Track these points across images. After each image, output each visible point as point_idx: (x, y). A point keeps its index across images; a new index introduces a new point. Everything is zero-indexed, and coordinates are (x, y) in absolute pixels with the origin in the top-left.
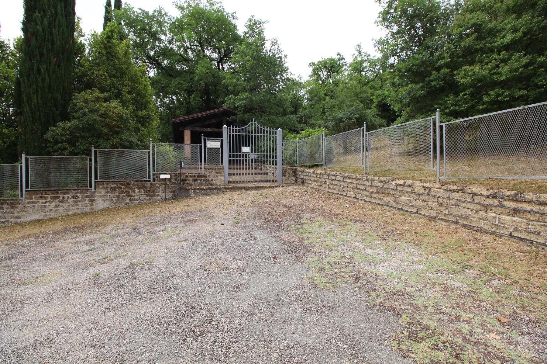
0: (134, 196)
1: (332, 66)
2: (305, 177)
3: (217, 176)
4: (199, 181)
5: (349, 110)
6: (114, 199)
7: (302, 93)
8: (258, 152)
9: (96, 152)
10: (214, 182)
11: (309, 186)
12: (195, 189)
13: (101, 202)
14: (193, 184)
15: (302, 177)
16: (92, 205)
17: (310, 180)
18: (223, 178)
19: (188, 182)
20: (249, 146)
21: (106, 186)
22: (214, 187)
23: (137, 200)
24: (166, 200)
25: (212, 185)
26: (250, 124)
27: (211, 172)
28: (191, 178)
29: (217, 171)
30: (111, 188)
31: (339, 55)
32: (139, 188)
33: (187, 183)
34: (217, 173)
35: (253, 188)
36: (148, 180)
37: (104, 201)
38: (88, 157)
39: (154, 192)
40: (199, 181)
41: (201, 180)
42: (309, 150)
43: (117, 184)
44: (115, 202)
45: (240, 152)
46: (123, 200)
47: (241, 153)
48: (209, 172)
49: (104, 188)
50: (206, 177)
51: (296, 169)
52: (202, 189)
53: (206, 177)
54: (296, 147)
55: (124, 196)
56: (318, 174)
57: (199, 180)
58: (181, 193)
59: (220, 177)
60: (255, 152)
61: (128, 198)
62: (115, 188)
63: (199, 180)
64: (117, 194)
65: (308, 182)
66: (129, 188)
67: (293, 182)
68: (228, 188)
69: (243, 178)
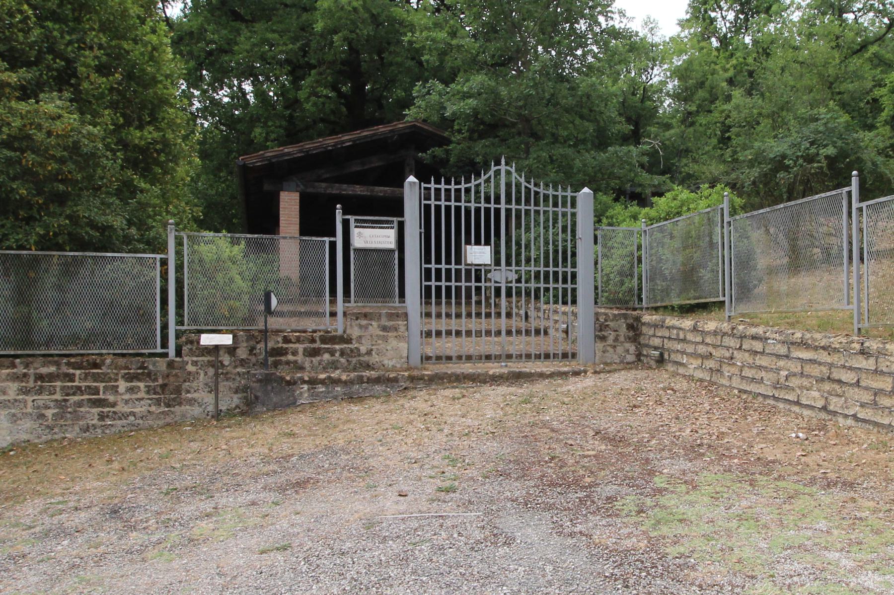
0: (114, 405)
2: (668, 344)
4: (326, 356)
6: (49, 413)
7: (657, 75)
8: (518, 263)
10: (374, 359)
11: (681, 370)
12: (313, 382)
14: (307, 365)
15: (657, 342)
19: (290, 357)
20: (487, 243)
21: (21, 370)
22: (374, 374)
23: (125, 416)
25: (368, 367)
26: (491, 173)
27: (366, 327)
28: (300, 347)
29: (385, 322)
30: (40, 377)
32: (130, 378)
33: (288, 363)
34: (384, 329)
36: (159, 350)
39: (178, 390)
40: (326, 356)
41: (332, 353)
42: (680, 259)
43: (58, 364)
44: (50, 422)
46: (77, 417)
47: (463, 267)
48: (361, 327)
50: (349, 341)
51: (638, 319)
53: (349, 341)
54: (639, 248)
55: (80, 404)
56: (709, 333)
59: (393, 343)
60: (508, 263)
61: (95, 411)
62: (51, 377)
64: (58, 396)
66: (96, 378)
67: (630, 358)
68: (421, 378)
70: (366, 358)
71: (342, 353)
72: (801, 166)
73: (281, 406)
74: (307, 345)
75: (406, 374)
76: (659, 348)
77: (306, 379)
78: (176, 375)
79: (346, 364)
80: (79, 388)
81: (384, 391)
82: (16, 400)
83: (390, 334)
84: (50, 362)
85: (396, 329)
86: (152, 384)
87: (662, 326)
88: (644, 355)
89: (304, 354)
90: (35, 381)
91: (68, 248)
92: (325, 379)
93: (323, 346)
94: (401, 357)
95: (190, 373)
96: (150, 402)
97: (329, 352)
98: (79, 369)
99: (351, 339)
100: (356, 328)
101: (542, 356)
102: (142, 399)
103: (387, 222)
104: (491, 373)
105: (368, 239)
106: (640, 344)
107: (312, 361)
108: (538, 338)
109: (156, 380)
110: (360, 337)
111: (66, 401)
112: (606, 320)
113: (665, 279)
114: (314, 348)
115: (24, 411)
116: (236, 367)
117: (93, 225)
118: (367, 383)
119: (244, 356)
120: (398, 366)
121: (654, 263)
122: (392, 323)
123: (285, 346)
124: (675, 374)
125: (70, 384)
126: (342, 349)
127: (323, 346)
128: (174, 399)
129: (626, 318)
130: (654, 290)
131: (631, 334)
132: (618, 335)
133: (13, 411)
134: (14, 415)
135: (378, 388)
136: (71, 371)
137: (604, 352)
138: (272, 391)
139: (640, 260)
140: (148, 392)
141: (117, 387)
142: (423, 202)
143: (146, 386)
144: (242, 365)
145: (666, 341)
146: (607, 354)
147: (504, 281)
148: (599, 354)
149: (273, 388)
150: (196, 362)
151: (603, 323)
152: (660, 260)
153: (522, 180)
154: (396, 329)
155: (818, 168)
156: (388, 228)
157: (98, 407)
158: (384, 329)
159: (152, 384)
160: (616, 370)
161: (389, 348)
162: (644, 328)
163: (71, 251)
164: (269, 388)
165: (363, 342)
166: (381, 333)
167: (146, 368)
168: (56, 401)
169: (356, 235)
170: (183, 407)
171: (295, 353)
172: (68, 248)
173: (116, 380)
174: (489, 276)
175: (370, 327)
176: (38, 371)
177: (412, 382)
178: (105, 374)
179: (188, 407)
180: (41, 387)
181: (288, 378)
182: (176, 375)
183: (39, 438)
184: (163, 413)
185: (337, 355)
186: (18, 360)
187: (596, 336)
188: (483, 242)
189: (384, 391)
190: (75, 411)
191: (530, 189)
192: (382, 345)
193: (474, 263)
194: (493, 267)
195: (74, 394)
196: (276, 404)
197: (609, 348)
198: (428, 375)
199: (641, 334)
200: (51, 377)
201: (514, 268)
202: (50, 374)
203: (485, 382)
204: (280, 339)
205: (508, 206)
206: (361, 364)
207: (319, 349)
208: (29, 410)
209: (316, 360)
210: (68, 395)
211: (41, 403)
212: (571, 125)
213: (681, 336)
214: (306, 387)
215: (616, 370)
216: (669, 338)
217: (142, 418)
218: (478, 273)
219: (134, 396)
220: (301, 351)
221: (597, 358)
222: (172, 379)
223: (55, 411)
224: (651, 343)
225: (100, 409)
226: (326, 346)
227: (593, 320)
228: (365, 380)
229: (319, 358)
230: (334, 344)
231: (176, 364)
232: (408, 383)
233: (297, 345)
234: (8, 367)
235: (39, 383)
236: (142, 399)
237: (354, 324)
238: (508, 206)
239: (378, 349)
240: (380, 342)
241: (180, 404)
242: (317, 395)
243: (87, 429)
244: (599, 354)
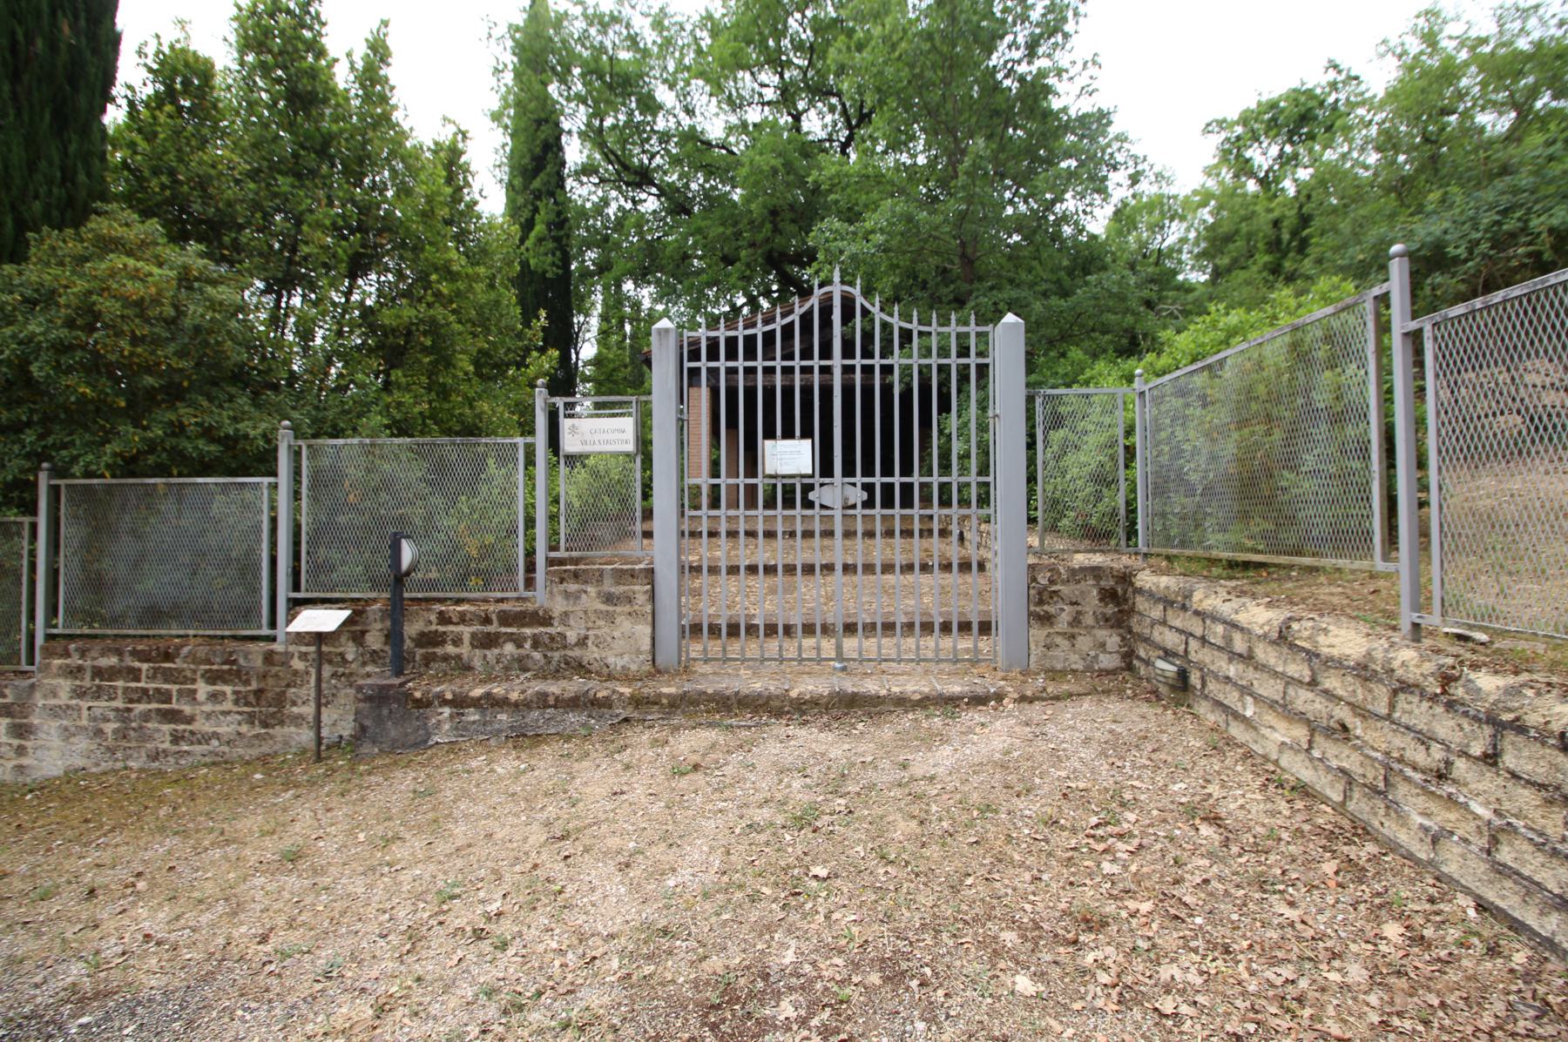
0: (190, 720)
1: (1301, 119)
2: (1198, 653)
3: (610, 618)
4: (509, 648)
5: (1489, 195)
6: (109, 728)
7: (1174, 232)
9: (55, 492)
10: (591, 654)
11: (1237, 731)
13: (56, 742)
14: (477, 663)
15: (1171, 639)
16: (21, 751)
17: (1246, 690)
19: (450, 649)
20: (807, 433)
21: (75, 660)
23: (206, 739)
24: (320, 752)
25: (581, 668)
27: (576, 597)
28: (466, 631)
29: (609, 586)
30: (98, 673)
31: (1335, 67)
32: (212, 678)
34: (609, 599)
35: (815, 702)
36: (265, 631)
37: (67, 734)
38: (26, 520)
39: (280, 700)
40: (509, 648)
41: (518, 642)
42: (1229, 448)
43: (119, 653)
44: (110, 742)
45: (752, 469)
46: (145, 737)
47: (759, 481)
49: (74, 672)
50: (547, 621)
51: (1126, 578)
52: (501, 703)
53: (547, 621)
55: (146, 717)
57: (511, 638)
58: (379, 721)
59: (625, 625)
60: (848, 470)
61: (167, 728)
62: (113, 673)
63: (511, 638)
64: (119, 704)
65: (1232, 698)
66: (169, 676)
67: (1108, 661)
69: (809, 598)
70: (577, 653)
71: (536, 644)
72: (1484, 256)
77: (449, 696)
78: (276, 675)
80: (145, 691)
81: (583, 725)
82: (68, 707)
83: (618, 609)
84: (110, 650)
85: (630, 600)
86: (242, 689)
88: (1139, 658)
90: (93, 679)
91: (175, 472)
92: (480, 699)
93: (503, 630)
94: (638, 652)
95: (296, 673)
96: (239, 717)
97: (514, 641)
98: (148, 661)
99: (551, 618)
100: (559, 599)
101: (955, 627)
102: (228, 713)
103: (621, 404)
104: (794, 694)
105: (588, 437)
106: (1130, 632)
107: (485, 656)
109: (247, 682)
110: (566, 614)
111: (129, 710)
112: (1052, 582)
113: (1191, 492)
115: (78, 723)
116: (364, 664)
117: (208, 433)
118: (555, 707)
119: (376, 646)
120: (634, 667)
121: (1164, 459)
122: (622, 588)
123: (441, 629)
124: (1220, 745)
125: (133, 685)
127: (503, 630)
128: (273, 715)
129: (1098, 578)
130: (1163, 515)
131: (1110, 609)
133: (65, 722)
134: (66, 729)
135: (572, 717)
136: (137, 664)
137: (1047, 647)
138: (389, 718)
140: (236, 702)
141: (194, 691)
142: (687, 365)
143: (235, 693)
145: (1194, 645)
146: (1054, 653)
147: (838, 505)
148: (1036, 651)
150: (306, 654)
151: (1045, 589)
152: (1178, 453)
153: (856, 291)
154: (630, 600)
155: (1529, 255)
156: (622, 415)
157: (170, 722)
159: (242, 689)
160: (1070, 695)
161: (616, 634)
163: (180, 475)
164: (385, 712)
165: (572, 622)
166: (603, 607)
167: (234, 662)
168: (117, 710)
170: (286, 729)
171: (457, 642)
172: (175, 472)
173: (194, 681)
174: (811, 496)
176: (96, 663)
177: (636, 707)
178: (180, 671)
179: (293, 729)
180: (99, 687)
181: (418, 695)
182: (276, 675)
183: (97, 765)
184: (257, 736)
185: (527, 645)
186: (72, 646)
187: (1030, 614)
188: (798, 433)
189: (583, 725)
190: (141, 728)
192: (604, 629)
193: (780, 472)
194: (817, 480)
195: (139, 701)
196: (394, 741)
197: (1059, 640)
198: (668, 696)
199: (1133, 610)
200: (113, 673)
201: (859, 479)
202: (112, 667)
203: (778, 713)
204: (433, 618)
205: (848, 362)
206: (567, 663)
207: (498, 635)
208: (84, 722)
209: (491, 654)
210: (131, 701)
211: (97, 712)
213: (1239, 645)
214: (447, 711)
215: (1070, 695)
216: (1203, 640)
217: (228, 743)
219: (218, 708)
220: (466, 638)
221: (1033, 659)
222: (270, 681)
223: (116, 725)
224: (1156, 636)
225: (173, 726)
226: (509, 630)
229: (496, 651)
230: (523, 626)
231: (276, 657)
232: (630, 709)
233: (460, 628)
234: (61, 656)
235: (97, 682)
236: (228, 713)
238: (848, 362)
239: (597, 636)
240: (602, 623)
241: (282, 723)
243: (155, 756)
244: (1036, 651)
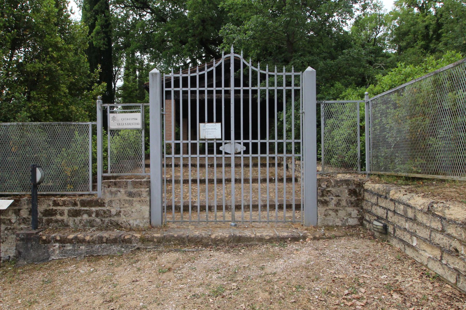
2: (392, 218)
3: (131, 203)
4: (85, 217)
7: (382, 31)
8: (246, 137)
10: (122, 219)
11: (409, 252)
12: (63, 241)
14: (71, 223)
17: (413, 234)
18: (146, 208)
19: (59, 217)
20: (219, 120)
22: (115, 233)
26: (222, 61)
27: (115, 193)
28: (66, 209)
29: (130, 189)
33: (57, 221)
34: (130, 194)
40: (85, 217)
41: (89, 214)
42: (407, 127)
45: (194, 136)
47: (198, 142)
48: (111, 193)
50: (102, 205)
51: (360, 185)
54: (362, 120)
56: (454, 222)
58: (27, 249)
59: (137, 206)
60: (237, 137)
67: (352, 222)
68: (150, 240)
70: (116, 219)
71: (97, 215)
73: (38, 261)
74: (71, 208)
75: (138, 235)
76: (382, 219)
77: (58, 238)
79: (100, 223)
81: (119, 251)
83: (134, 199)
87: (386, 198)
89: (68, 215)
92: (72, 239)
93: (83, 208)
94: (144, 218)
99: (104, 203)
100: (108, 194)
104: (213, 237)
105: (120, 122)
106: (362, 208)
107: (74, 220)
108: (290, 185)
110: (111, 201)
112: (328, 186)
113: (389, 146)
114: (76, 210)
116: (20, 224)
118: (106, 243)
119: (25, 216)
120: (141, 225)
121: (377, 132)
122: (136, 190)
123: (55, 208)
126: (97, 211)
127: (83, 208)
129: (348, 185)
131: (353, 199)
132: (339, 200)
135: (114, 248)
137: (326, 215)
138: (31, 248)
139: (362, 129)
144: (24, 223)
145: (390, 214)
146: (328, 218)
147: (233, 152)
148: (321, 217)
149: (32, 245)
151: (325, 190)
152: (383, 129)
158: (130, 194)
160: (336, 237)
161: (133, 210)
162: (366, 194)
164: (30, 245)
165: (113, 205)
166: (128, 198)
169: (111, 119)
171: (62, 214)
174: (221, 148)
175: (119, 193)
181: (44, 238)
185: (94, 215)
187: (318, 201)
189: (119, 251)
191: (256, 72)
194: (223, 141)
196: (34, 258)
197: (330, 212)
198: (157, 238)
201: (242, 141)
203: (206, 245)
204: (51, 203)
206: (111, 223)
207: (80, 211)
209: (77, 219)
212: (320, 44)
214: (57, 245)
215: (336, 237)
216: (394, 212)
218: (212, 147)
220: (66, 212)
221: (319, 221)
224: (374, 211)
226: (85, 208)
227: (315, 185)
228: (105, 241)
229: (79, 218)
230: (91, 206)
232: (140, 244)
233: (63, 208)
237: (106, 191)
239: (125, 211)
240: (127, 205)
242: (66, 253)
